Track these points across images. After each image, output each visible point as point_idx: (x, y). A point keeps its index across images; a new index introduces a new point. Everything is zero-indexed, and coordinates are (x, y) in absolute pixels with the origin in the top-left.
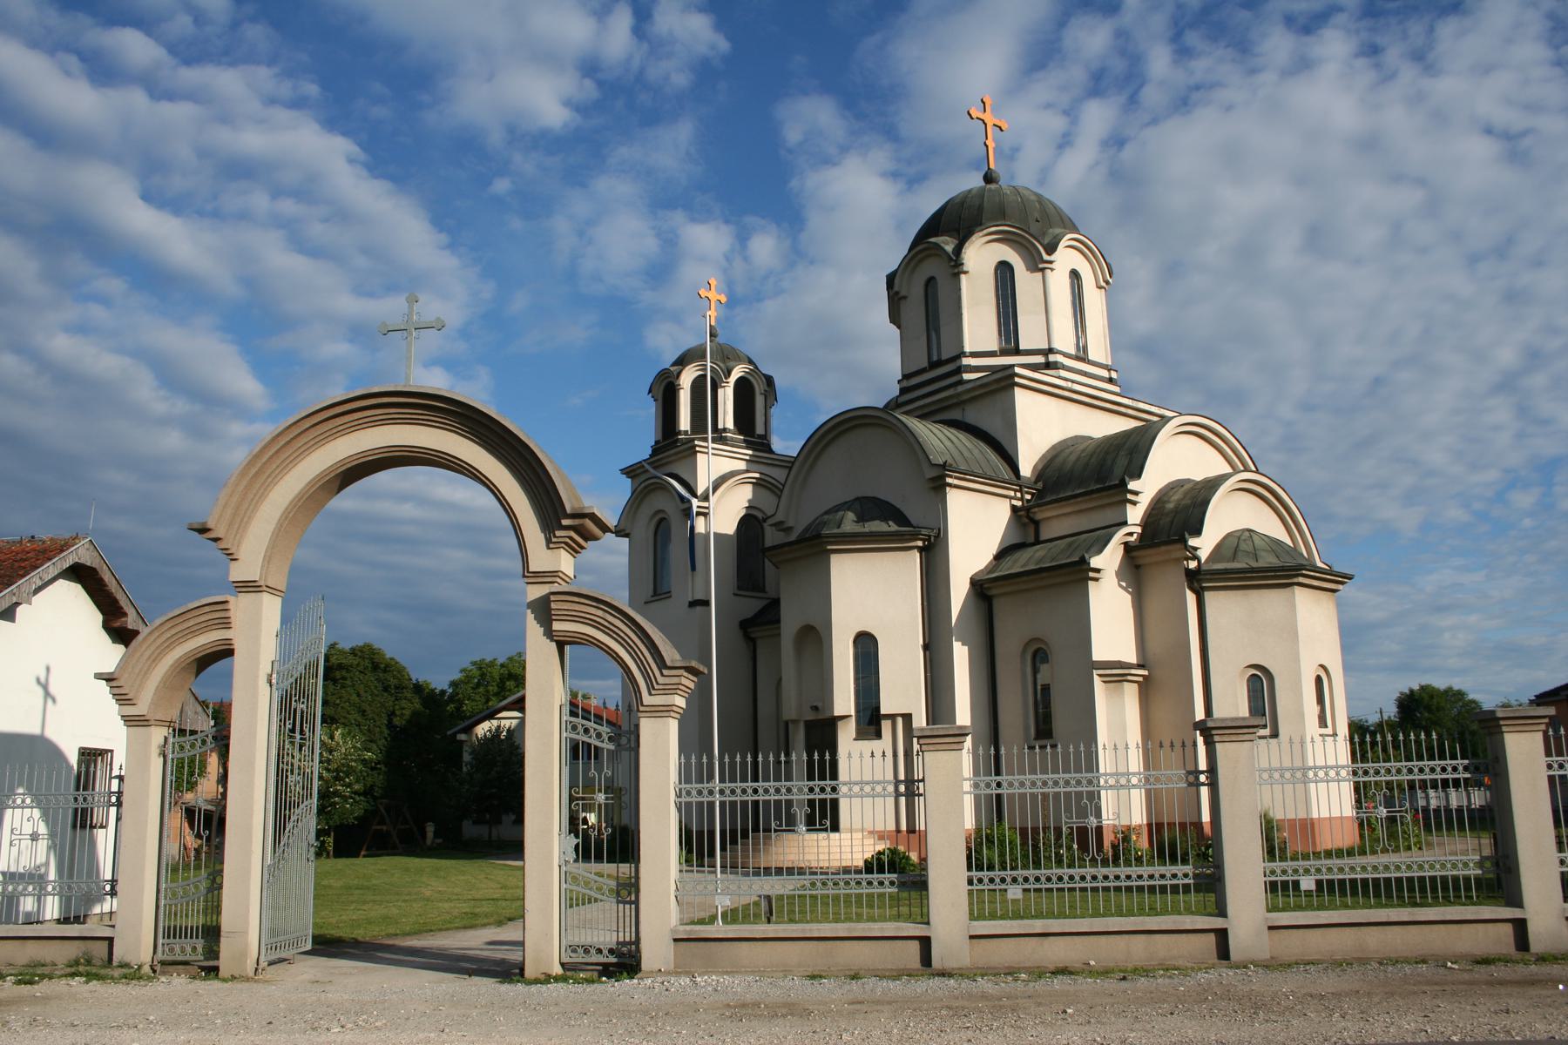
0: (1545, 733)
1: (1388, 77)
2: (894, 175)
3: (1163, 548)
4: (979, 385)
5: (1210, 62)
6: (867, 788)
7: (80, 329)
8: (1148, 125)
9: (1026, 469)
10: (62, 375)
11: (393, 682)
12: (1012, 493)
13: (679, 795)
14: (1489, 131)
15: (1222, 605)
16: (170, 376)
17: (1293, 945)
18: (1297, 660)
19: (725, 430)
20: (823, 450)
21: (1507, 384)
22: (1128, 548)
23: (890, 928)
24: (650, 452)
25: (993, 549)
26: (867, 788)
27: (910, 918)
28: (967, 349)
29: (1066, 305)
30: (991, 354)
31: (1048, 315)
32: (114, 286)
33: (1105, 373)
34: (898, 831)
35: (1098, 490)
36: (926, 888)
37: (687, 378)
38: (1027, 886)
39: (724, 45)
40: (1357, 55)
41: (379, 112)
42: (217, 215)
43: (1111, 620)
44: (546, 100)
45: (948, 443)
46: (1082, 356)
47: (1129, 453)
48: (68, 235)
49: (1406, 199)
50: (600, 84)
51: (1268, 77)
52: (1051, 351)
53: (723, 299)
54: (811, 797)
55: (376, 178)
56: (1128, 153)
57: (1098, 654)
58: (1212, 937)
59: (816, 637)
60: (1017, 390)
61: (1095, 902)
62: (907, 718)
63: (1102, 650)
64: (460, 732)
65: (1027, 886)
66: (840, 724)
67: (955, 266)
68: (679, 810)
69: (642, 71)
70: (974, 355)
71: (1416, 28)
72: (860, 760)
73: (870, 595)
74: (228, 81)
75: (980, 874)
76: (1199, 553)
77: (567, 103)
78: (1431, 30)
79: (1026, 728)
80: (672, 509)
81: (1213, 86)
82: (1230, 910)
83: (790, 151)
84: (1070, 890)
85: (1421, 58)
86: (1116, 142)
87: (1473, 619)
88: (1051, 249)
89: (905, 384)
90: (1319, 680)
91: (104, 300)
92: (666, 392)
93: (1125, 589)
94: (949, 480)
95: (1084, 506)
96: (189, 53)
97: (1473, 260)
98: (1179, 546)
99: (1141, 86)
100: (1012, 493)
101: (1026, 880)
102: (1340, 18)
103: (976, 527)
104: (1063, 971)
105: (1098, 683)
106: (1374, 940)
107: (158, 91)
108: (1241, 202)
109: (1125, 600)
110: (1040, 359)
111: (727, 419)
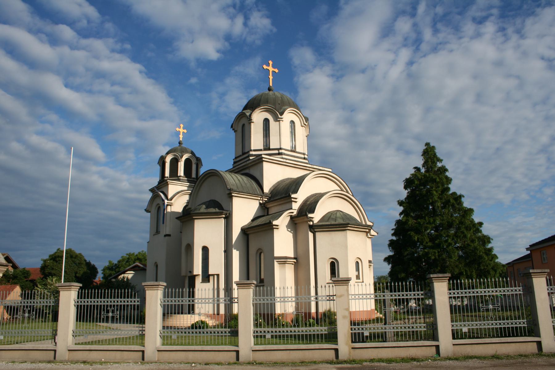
0: (78, 292)
1: (507, 39)
2: (332, 76)
3: (302, 218)
4: (254, 161)
5: (445, 33)
6: (205, 301)
7: (41, 133)
8: (421, 57)
9: (266, 189)
10: (34, 150)
11: (77, 262)
13: (253, 301)
14: (543, 58)
15: (323, 238)
17: (261, 356)
18: (347, 256)
19: (180, 176)
20: (203, 183)
21: (544, 150)
22: (292, 218)
24: (157, 183)
25: (251, 218)
26: (205, 301)
27: (230, 344)
28: (252, 148)
29: (289, 132)
31: (281, 136)
32: (54, 117)
33: (303, 156)
34: (214, 314)
37: (168, 159)
39: (275, 30)
40: (498, 32)
41: (150, 54)
43: (283, 242)
44: (209, 49)
45: (237, 181)
47: (294, 185)
48: (39, 99)
49: (512, 83)
50: (231, 44)
51: (466, 40)
52: (281, 149)
53: (185, 131)
54: (391, 298)
55: (149, 78)
56: (414, 67)
57: (276, 255)
59: (190, 248)
61: (222, 340)
62: (218, 275)
63: (278, 253)
64: (113, 278)
66: (196, 277)
67: (250, 120)
68: (253, 306)
69: (245, 40)
70: (255, 150)
71: (518, 21)
72: (203, 290)
73: (207, 233)
74: (98, 44)
75: (355, 327)
76: (313, 219)
77: (218, 51)
78: (524, 21)
80: (161, 203)
81: (446, 43)
83: (295, 67)
85: (520, 33)
86: (410, 63)
87: (529, 234)
88: (282, 114)
89: (235, 160)
90: (357, 263)
91: (51, 123)
92: (162, 162)
93: (290, 232)
94: (233, 194)
95: (278, 203)
96: (84, 34)
97: (535, 105)
99: (421, 43)
101: (469, 325)
102: (492, 18)
103: (244, 210)
104: (84, 362)
105: (276, 264)
106: (413, 352)
107: (73, 47)
108: (452, 85)
110: (276, 152)
111: (181, 172)
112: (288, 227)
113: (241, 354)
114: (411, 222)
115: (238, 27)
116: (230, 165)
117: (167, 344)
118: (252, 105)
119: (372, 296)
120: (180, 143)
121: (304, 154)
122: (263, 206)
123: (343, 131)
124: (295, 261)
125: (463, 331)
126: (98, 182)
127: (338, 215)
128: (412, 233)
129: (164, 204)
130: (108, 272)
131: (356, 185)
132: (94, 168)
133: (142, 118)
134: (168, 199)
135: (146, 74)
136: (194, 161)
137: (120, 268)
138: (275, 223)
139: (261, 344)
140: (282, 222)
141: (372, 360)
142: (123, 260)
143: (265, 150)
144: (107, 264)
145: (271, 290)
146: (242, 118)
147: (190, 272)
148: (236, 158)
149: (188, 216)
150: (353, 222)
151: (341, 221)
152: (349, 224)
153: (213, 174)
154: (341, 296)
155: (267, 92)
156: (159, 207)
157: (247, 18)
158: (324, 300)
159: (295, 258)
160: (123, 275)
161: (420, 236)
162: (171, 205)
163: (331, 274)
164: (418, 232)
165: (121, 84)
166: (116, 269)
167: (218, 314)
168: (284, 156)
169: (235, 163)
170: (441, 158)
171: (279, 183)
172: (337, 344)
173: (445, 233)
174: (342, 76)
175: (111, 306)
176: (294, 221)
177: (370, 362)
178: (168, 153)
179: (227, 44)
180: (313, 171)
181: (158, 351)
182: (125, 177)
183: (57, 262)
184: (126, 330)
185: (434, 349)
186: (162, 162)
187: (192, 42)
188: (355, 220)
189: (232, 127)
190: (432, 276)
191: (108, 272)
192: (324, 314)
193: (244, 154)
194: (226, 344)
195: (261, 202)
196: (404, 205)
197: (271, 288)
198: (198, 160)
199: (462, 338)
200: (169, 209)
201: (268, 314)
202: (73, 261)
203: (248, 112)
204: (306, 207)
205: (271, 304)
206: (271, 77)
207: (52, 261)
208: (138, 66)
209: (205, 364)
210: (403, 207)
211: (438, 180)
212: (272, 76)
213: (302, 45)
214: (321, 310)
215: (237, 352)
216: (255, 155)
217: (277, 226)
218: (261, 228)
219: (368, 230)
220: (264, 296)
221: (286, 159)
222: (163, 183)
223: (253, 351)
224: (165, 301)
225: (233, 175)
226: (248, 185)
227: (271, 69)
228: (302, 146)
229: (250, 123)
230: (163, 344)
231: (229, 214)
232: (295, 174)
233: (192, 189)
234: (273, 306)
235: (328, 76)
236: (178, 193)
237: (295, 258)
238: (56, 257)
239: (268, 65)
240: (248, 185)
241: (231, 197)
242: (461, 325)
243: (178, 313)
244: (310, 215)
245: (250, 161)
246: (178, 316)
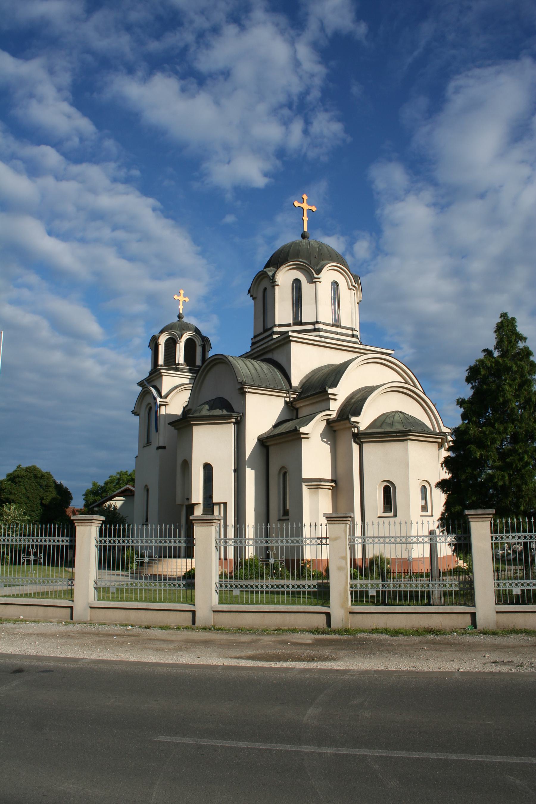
2: (434, 205)
3: (342, 422)
7: (16, 302)
9: (296, 381)
11: (44, 483)
12: (285, 395)
16: (58, 325)
17: (225, 620)
19: (179, 364)
22: (329, 423)
23: (179, 606)
27: (186, 602)
28: (277, 323)
29: (331, 298)
30: (288, 325)
31: (319, 302)
32: (33, 278)
33: (350, 332)
35: (314, 395)
36: (194, 589)
37: (162, 340)
38: (242, 589)
39: (349, 139)
42: (83, 241)
43: (315, 457)
44: (251, 170)
45: (253, 371)
46: (337, 324)
47: (335, 374)
48: (19, 254)
52: (317, 323)
53: (187, 299)
55: (167, 217)
57: (305, 475)
58: (469, 615)
60: (292, 343)
62: (225, 504)
64: (95, 506)
65: (242, 589)
66: (195, 507)
67: (273, 283)
70: (280, 326)
73: (211, 445)
74: (94, 173)
76: (359, 425)
79: (279, 511)
80: (152, 401)
82: (75, 598)
83: (378, 193)
84: (246, 591)
88: (319, 272)
89: (254, 340)
90: (424, 487)
91: (30, 287)
92: (154, 344)
94: (246, 390)
96: (75, 157)
98: (347, 421)
100: (285, 395)
101: (522, 585)
103: (263, 412)
105: (305, 490)
107: (58, 178)
109: (325, 449)
110: (311, 327)
111: (180, 358)
112: (323, 435)
113: (197, 615)
114: (473, 431)
115: (296, 135)
116: (247, 348)
117: (104, 599)
118: (277, 260)
119: (426, 539)
120: (180, 317)
121: (352, 329)
122: (291, 408)
123: (448, 287)
124: (334, 485)
125: (514, 593)
126: (92, 368)
127: (397, 417)
128: (473, 447)
129: (156, 403)
130: (92, 498)
131: (419, 375)
132: (88, 350)
133: (155, 277)
134: (161, 397)
135: (162, 211)
136: (198, 342)
137: (107, 492)
138: (302, 430)
139: (267, 603)
140: (314, 429)
141: (373, 631)
142: (112, 481)
143: (295, 324)
144: (90, 486)
145: (297, 528)
146: (262, 279)
147: (188, 499)
148: (255, 337)
149: (184, 423)
150: (419, 429)
151: (400, 428)
152: (410, 431)
153: (221, 360)
154: (336, 539)
155: (300, 238)
156: (151, 408)
157: (307, 123)
158: (313, 545)
159: (333, 481)
160: (108, 503)
161: (484, 452)
162: (165, 405)
163: (384, 504)
164: (481, 445)
165: (126, 228)
166: (102, 493)
167: (225, 559)
168: (322, 334)
169: (253, 344)
170: (525, 335)
171: (315, 372)
172: (329, 607)
173: (521, 448)
174: (448, 205)
175: (33, 546)
176: (332, 427)
177: (370, 632)
178: (162, 332)
179: (278, 163)
180: (365, 354)
181: (91, 607)
182: (131, 361)
183: (16, 483)
184: (113, 581)
185: (468, 618)
186: (154, 344)
187: (229, 162)
188: (423, 425)
189: (249, 292)
190: (467, 512)
191: (92, 498)
192: (371, 561)
193: (265, 330)
194: (179, 602)
195: (287, 399)
196: (465, 405)
197: (297, 525)
198: (206, 342)
199: (511, 603)
200: (163, 411)
201: (293, 561)
202: (37, 483)
203: (270, 271)
204: (349, 408)
205: (298, 547)
206: (306, 219)
207: (9, 482)
208: (151, 201)
209: (146, 628)
210: (464, 409)
211: (515, 368)
212: (308, 217)
213: (390, 160)
214: (370, 555)
215: (194, 612)
216: (280, 333)
217: (307, 434)
218: (283, 440)
219: (440, 440)
220: (282, 536)
221: (325, 337)
222: (155, 375)
223: (214, 611)
224: (101, 541)
225: (248, 362)
226: (269, 375)
227: (305, 206)
228: (350, 316)
229: (273, 287)
230: (221, 603)
231: (241, 417)
232: (336, 358)
233: (192, 382)
234: (300, 550)
235: (428, 206)
236: (176, 387)
237: (333, 481)
238: (14, 477)
239: (179, 294)
240: (269, 375)
241: (243, 394)
242: (511, 585)
243: (170, 557)
244: (353, 419)
245: (273, 342)
246: (170, 560)
